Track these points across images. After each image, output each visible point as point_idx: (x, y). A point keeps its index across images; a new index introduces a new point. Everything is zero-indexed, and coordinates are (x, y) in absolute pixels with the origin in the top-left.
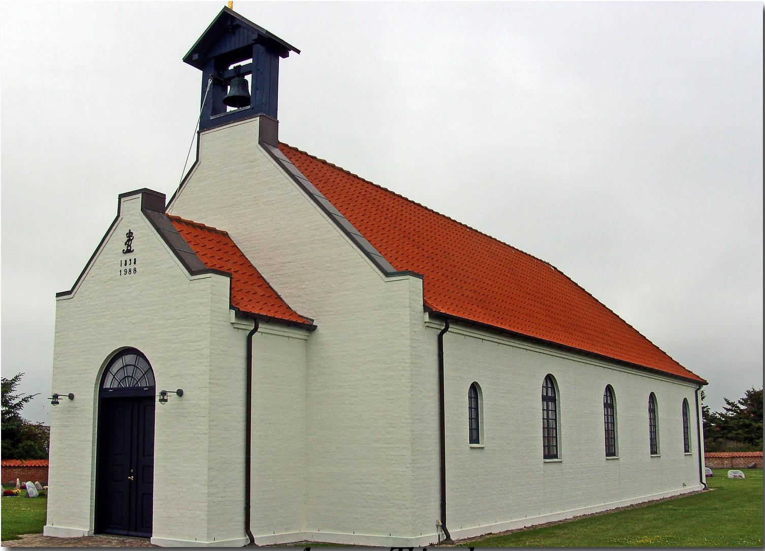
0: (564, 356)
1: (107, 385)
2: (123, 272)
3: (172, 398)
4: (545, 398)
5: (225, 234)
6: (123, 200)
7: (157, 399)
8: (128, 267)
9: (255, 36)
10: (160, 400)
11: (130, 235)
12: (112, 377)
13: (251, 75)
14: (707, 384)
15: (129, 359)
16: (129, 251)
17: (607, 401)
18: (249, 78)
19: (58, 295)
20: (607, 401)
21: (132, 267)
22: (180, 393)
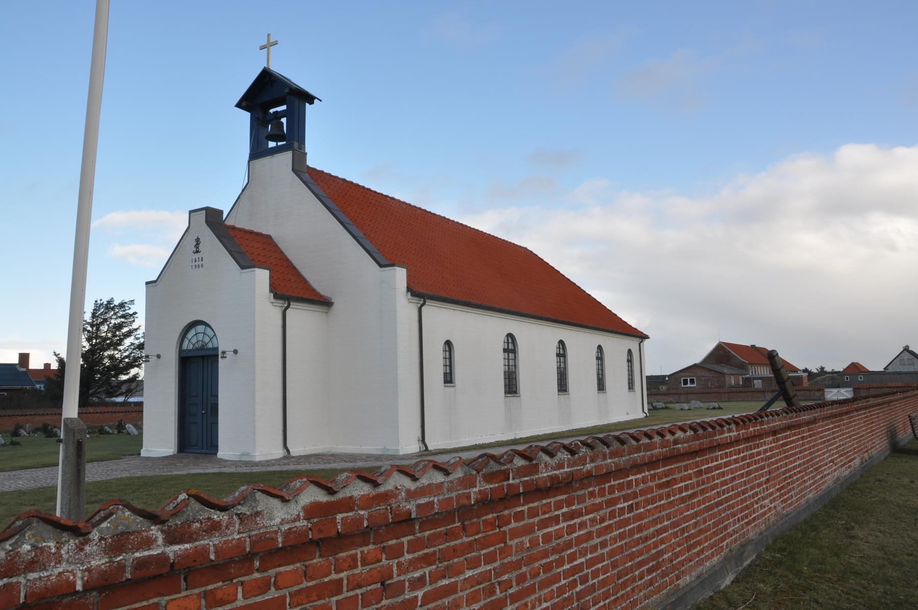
0: (531, 322)
1: (185, 347)
2: (194, 267)
3: (229, 355)
4: (558, 355)
5: (269, 237)
6: (192, 214)
7: (220, 356)
8: (197, 263)
9: (287, 90)
10: (222, 357)
11: (198, 240)
12: (188, 341)
13: (269, 147)
14: (648, 338)
15: (200, 328)
16: (197, 252)
17: (560, 351)
18: (284, 120)
19: (147, 283)
20: (560, 351)
21: (200, 263)
22: (235, 352)
